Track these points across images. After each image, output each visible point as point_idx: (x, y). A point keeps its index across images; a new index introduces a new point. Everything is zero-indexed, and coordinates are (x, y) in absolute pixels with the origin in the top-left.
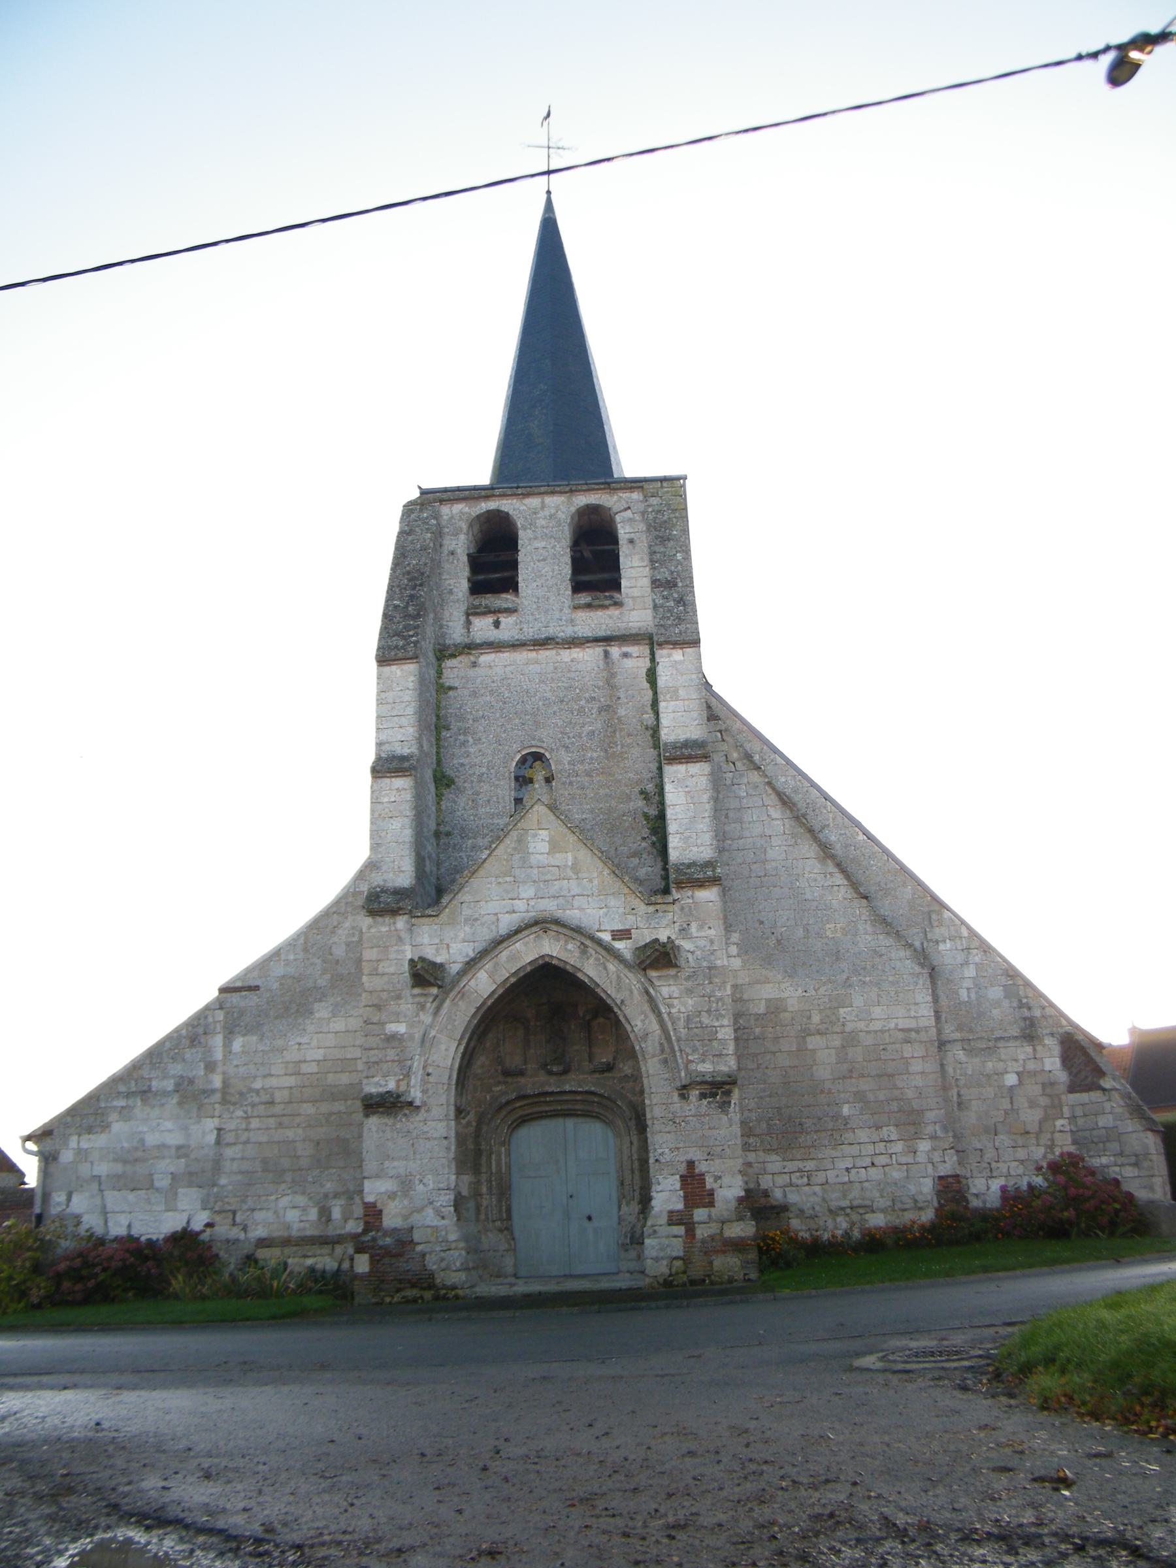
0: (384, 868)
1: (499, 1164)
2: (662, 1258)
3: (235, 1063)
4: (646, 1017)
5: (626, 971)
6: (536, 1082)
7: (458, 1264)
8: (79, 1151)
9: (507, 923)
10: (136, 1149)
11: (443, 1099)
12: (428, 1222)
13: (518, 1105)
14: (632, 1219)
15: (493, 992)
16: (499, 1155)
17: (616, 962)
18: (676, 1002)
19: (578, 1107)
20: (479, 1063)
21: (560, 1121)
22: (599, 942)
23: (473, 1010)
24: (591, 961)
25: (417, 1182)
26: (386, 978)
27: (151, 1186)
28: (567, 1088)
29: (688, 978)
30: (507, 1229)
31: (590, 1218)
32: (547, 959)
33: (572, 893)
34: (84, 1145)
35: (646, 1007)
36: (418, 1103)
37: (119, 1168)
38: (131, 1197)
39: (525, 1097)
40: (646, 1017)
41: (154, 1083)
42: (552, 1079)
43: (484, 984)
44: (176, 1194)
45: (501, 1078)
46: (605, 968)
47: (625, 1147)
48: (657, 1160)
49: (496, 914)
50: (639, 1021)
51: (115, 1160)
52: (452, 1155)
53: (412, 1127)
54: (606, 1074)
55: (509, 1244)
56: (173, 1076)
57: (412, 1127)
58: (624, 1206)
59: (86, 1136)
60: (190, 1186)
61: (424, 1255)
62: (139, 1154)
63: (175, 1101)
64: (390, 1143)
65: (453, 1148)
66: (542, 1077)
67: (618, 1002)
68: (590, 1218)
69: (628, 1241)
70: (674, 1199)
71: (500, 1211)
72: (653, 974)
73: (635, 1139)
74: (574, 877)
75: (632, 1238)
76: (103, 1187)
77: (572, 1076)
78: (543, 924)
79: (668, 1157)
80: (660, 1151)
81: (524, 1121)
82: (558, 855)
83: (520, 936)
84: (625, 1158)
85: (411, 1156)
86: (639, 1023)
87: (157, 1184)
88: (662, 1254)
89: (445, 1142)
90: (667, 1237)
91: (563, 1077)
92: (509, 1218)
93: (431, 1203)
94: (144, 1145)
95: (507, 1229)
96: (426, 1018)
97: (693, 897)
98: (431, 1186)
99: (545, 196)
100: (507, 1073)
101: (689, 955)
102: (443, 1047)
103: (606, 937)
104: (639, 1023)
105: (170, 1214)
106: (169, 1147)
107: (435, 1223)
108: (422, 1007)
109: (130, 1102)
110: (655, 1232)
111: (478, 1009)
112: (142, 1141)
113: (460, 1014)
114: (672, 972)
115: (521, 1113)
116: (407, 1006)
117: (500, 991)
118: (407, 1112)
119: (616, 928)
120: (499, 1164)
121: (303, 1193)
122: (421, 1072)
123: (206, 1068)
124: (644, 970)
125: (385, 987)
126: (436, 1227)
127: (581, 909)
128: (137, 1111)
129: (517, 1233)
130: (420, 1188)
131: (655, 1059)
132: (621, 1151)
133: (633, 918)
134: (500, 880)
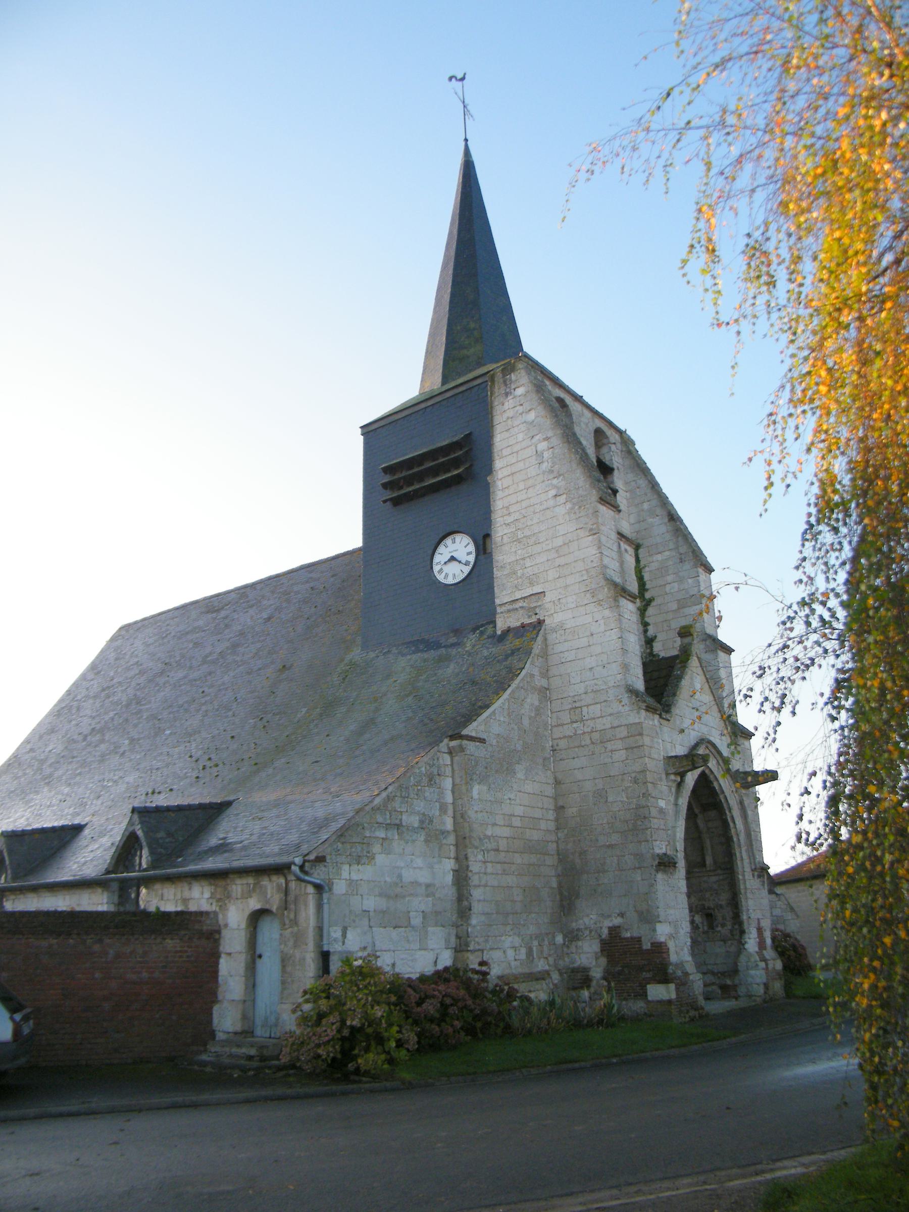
3: (475, 808)
8: (351, 883)
10: (396, 884)
27: (409, 925)
34: (355, 877)
37: (382, 903)
38: (394, 934)
41: (404, 817)
44: (427, 932)
51: (380, 895)
56: (418, 813)
59: (355, 867)
60: (436, 925)
62: (399, 890)
63: (422, 838)
76: (372, 924)
87: (413, 922)
94: (401, 880)
99: (463, 143)
105: (423, 952)
106: (420, 884)
109: (389, 834)
112: (400, 876)
121: (519, 935)
123: (441, 809)
128: (395, 844)
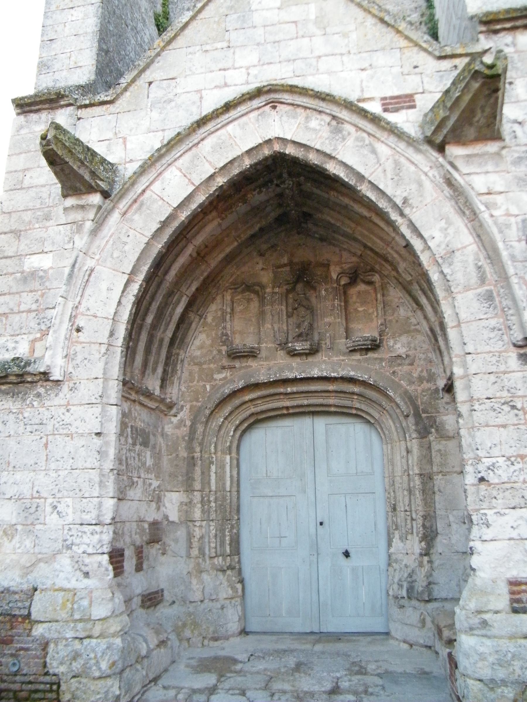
0: (57, 66)
1: (220, 478)
2: (504, 683)
4: (449, 223)
5: (410, 152)
6: (273, 365)
7: (104, 665)
9: (213, 101)
11: (98, 370)
12: (61, 583)
13: (247, 398)
14: (411, 561)
15: (189, 198)
16: (223, 467)
17: (392, 140)
18: (499, 199)
19: (331, 401)
20: (197, 342)
21: (307, 421)
22: (364, 113)
23: (156, 226)
24: (350, 142)
25: (49, 509)
26: (32, 193)
28: (316, 373)
29: (519, 161)
30: (234, 568)
31: (347, 554)
32: (277, 147)
33: (317, 53)
35: (449, 208)
36: (56, 375)
39: (257, 386)
40: (449, 223)
42: (295, 362)
43: (177, 188)
45: (225, 362)
46: (374, 151)
47: (397, 458)
48: (482, 480)
49: (199, 91)
50: (434, 228)
52: (109, 464)
53: (47, 414)
54: (370, 355)
55: (233, 588)
57: (47, 414)
58: (396, 541)
61: (45, 646)
64: (12, 443)
65: (112, 452)
66: (281, 359)
67: (399, 201)
68: (347, 554)
69: (404, 593)
70: (518, 556)
71: (222, 543)
72: (453, 150)
73: (414, 445)
74: (319, 32)
75: (410, 590)
77: (320, 357)
78: (268, 95)
79: (504, 472)
80: (488, 462)
81: (258, 422)
82: (294, 8)
83: (233, 114)
84: (399, 471)
85: (42, 463)
86: (437, 234)
88: (501, 674)
89: (97, 442)
90: (512, 637)
91: (310, 359)
92: (236, 549)
93: (69, 548)
95: (231, 567)
96: (81, 241)
97: (514, 44)
98: (70, 519)
100: (235, 355)
101: (516, 127)
102: (104, 286)
103: (374, 108)
104: (437, 234)
107: (73, 584)
108: (78, 226)
110: (485, 624)
111: (164, 224)
113: (130, 237)
114: (492, 147)
115: (253, 410)
116: (56, 232)
117: (201, 198)
118: (42, 390)
119: (389, 94)
120: (220, 478)
122: (66, 325)
124: (441, 149)
125: (31, 205)
126: (74, 592)
127: (329, 73)
129: (247, 573)
130: (53, 520)
131: (471, 294)
132: (391, 462)
133: (417, 79)
134: (208, 47)
